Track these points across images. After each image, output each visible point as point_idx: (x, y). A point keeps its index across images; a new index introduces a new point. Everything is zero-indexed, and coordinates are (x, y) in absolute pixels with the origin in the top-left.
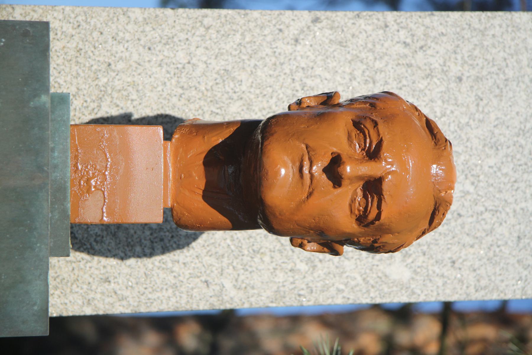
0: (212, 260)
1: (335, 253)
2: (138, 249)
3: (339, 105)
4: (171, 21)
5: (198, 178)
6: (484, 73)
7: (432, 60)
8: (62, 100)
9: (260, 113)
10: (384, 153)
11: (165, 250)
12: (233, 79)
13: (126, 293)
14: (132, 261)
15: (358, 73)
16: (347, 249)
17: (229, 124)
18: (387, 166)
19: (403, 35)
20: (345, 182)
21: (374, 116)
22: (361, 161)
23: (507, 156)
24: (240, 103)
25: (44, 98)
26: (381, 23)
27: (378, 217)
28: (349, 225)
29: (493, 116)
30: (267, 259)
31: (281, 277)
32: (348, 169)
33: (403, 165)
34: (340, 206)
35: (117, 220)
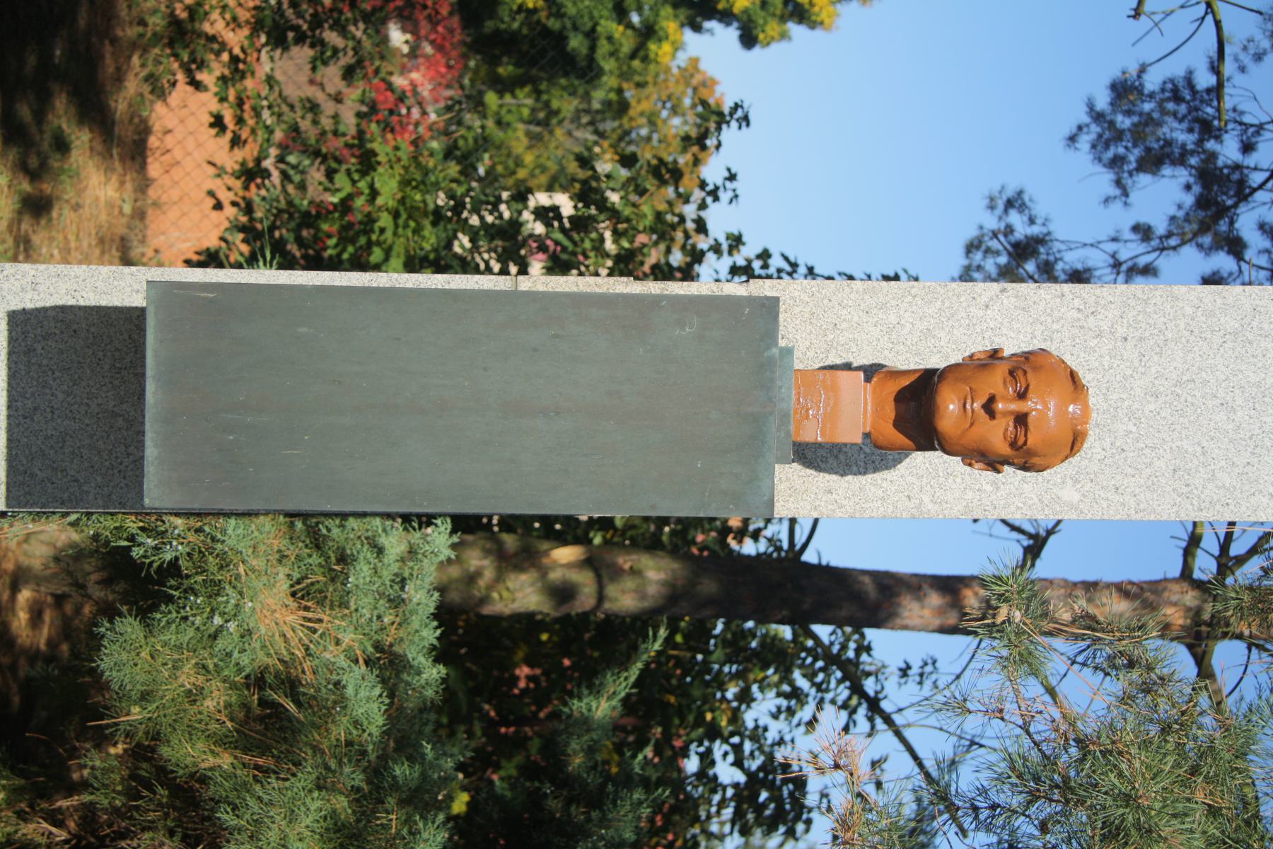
0: (914, 480)
1: (998, 472)
2: (855, 468)
3: (1002, 358)
4: (885, 291)
5: (890, 411)
6: (1147, 334)
7: (1101, 323)
8: (789, 352)
9: (937, 362)
10: (1030, 395)
11: (876, 470)
12: (934, 337)
13: (844, 503)
14: (850, 478)
15: (1038, 333)
16: (1006, 467)
17: (915, 371)
18: (1032, 405)
19: (1077, 302)
20: (998, 416)
21: (1026, 368)
22: (1012, 401)
23: (1165, 403)
24: (938, 356)
25: (775, 351)
26: (1058, 293)
27: (1025, 443)
28: (1004, 449)
29: (1153, 370)
30: (958, 480)
31: (970, 495)
32: (1000, 406)
33: (1046, 407)
34: (996, 435)
35: (827, 440)
